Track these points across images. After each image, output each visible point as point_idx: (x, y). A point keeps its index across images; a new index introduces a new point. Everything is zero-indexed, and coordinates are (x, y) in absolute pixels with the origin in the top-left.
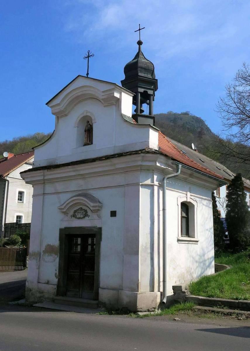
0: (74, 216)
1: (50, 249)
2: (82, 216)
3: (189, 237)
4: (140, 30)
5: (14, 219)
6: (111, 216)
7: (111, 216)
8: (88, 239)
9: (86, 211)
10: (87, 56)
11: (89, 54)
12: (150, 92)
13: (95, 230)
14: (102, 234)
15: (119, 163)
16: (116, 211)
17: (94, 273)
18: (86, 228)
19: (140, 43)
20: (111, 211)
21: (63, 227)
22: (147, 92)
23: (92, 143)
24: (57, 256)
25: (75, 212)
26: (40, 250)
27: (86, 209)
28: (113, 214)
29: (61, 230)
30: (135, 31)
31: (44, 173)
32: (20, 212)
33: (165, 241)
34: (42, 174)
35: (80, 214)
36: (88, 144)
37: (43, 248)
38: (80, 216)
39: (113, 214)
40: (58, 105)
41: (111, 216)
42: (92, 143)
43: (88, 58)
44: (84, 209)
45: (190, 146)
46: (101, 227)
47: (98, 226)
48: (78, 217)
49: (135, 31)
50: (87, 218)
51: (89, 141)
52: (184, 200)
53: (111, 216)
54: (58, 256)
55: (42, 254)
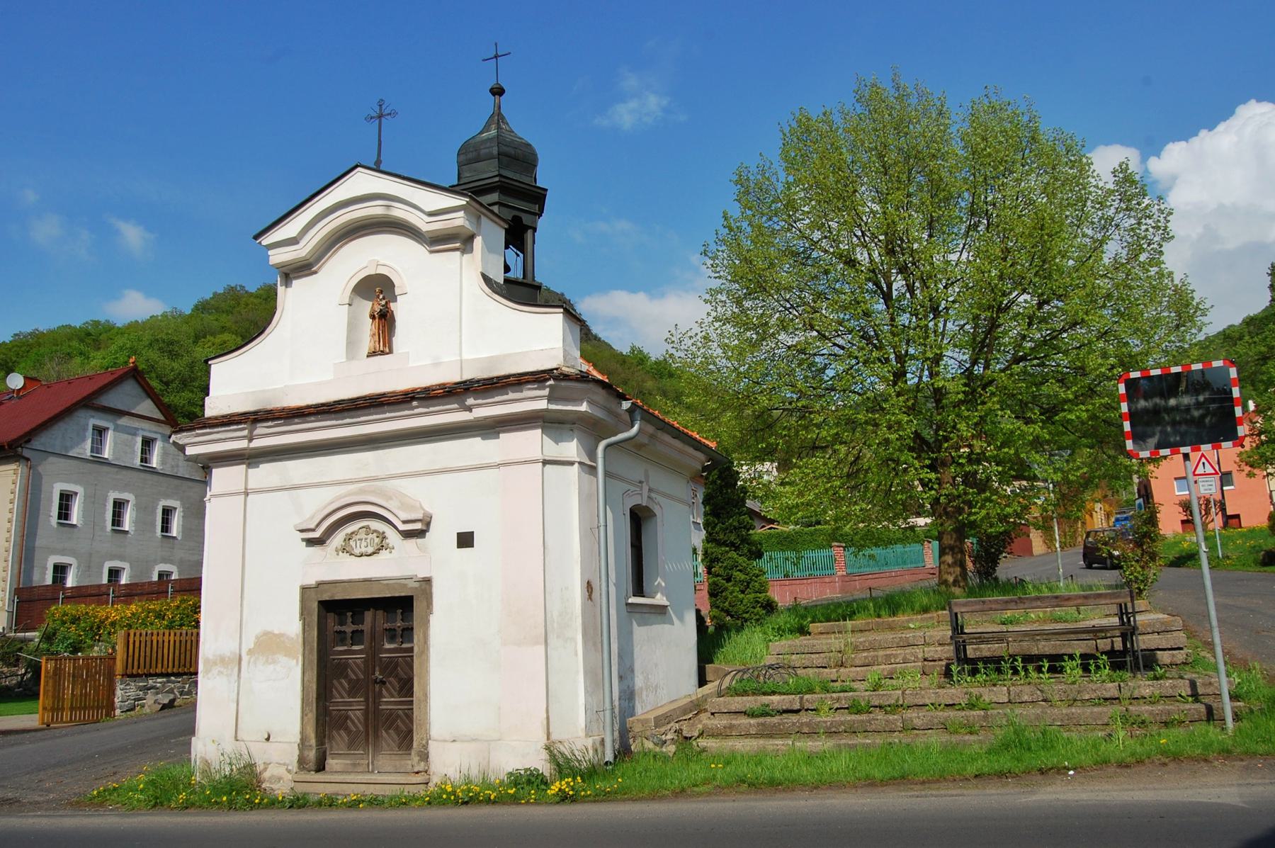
1: (268, 644)
2: (370, 550)
3: (643, 596)
4: (496, 57)
5: (45, 574)
6: (459, 535)
9: (383, 537)
10: (375, 115)
11: (381, 110)
12: (526, 219)
13: (412, 584)
14: (434, 596)
16: (473, 532)
17: (412, 701)
18: (456, 406)
19: (498, 91)
21: (311, 581)
22: (520, 219)
23: (391, 352)
24: (295, 661)
25: (349, 538)
26: (240, 649)
27: (381, 531)
28: (465, 540)
29: (304, 589)
30: (484, 60)
31: (251, 432)
32: (63, 552)
35: (364, 544)
36: (383, 353)
37: (249, 643)
38: (363, 550)
39: (465, 540)
40: (293, 241)
41: (458, 547)
42: (391, 352)
43: (377, 121)
44: (375, 531)
45: (201, 403)
46: (428, 576)
47: (422, 574)
48: (357, 551)
49: (484, 60)
50: (384, 554)
51: (384, 345)
52: (636, 500)
53: (459, 535)
55: (245, 658)
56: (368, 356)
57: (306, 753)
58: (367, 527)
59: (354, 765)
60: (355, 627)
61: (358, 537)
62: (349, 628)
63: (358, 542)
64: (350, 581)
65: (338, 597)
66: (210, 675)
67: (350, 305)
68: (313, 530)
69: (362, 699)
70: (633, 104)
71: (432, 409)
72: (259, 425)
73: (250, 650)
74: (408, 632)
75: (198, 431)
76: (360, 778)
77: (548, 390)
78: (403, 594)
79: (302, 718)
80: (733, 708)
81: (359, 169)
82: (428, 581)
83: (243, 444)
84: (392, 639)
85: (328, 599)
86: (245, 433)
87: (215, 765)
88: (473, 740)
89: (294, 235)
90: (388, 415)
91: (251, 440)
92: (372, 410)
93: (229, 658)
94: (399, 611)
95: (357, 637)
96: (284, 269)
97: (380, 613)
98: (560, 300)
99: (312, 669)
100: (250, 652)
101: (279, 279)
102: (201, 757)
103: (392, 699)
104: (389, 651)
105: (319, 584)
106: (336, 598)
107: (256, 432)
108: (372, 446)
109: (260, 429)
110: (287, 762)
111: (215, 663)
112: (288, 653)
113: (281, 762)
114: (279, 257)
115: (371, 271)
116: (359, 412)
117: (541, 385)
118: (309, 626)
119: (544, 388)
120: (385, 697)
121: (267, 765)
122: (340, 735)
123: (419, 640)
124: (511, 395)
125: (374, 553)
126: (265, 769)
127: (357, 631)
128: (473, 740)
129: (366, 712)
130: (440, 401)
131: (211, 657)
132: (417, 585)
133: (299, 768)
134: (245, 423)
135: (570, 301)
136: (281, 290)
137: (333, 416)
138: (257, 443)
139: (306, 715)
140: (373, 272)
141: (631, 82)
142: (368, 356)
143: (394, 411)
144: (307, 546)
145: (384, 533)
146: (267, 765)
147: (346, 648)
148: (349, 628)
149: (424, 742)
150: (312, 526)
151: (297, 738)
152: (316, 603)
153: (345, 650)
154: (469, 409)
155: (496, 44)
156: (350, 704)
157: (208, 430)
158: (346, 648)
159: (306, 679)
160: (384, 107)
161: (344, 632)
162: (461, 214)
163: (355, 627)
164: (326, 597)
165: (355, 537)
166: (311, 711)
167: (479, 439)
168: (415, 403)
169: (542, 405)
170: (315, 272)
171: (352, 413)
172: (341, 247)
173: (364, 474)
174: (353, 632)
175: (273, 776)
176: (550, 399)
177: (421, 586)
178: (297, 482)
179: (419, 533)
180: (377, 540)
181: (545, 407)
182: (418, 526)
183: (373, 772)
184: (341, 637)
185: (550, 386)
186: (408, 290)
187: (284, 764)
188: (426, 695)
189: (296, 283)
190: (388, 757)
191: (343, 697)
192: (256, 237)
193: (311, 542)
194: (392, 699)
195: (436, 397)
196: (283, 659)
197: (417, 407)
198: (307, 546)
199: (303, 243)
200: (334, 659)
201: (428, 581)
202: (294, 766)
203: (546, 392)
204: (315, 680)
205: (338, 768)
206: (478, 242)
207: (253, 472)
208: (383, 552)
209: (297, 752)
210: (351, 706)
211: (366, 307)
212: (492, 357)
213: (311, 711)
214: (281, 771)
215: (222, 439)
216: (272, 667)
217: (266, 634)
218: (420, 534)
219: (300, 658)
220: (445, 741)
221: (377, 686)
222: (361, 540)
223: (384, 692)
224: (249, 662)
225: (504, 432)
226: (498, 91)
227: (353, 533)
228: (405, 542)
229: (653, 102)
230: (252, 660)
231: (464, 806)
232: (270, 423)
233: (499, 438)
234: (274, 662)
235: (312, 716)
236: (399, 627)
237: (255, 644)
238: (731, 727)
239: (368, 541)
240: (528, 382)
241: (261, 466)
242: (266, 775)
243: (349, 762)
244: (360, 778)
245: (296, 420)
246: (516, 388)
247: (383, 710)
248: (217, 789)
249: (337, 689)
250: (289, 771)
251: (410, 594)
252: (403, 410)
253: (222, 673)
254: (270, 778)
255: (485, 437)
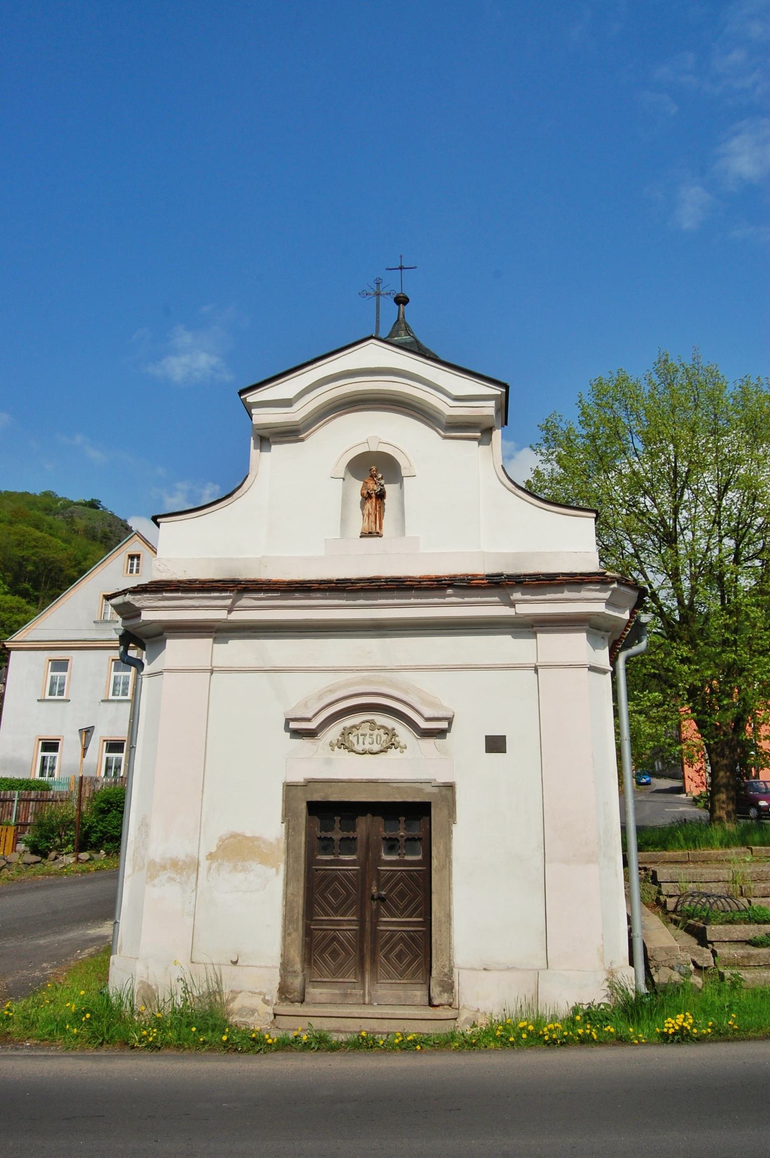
0: (343, 744)
2: (376, 748)
4: (401, 268)
6: (488, 738)
7: (486, 736)
8: (383, 859)
9: (391, 733)
11: (378, 288)
13: (428, 789)
15: (359, 669)
16: (486, 736)
18: (496, 599)
20: (486, 752)
24: (274, 870)
25: (347, 732)
27: (390, 728)
28: (496, 744)
29: (289, 787)
30: (388, 269)
33: (469, 589)
34: (228, 602)
35: (368, 740)
38: (367, 747)
40: (287, 403)
44: (383, 727)
47: (442, 779)
53: (488, 738)
54: (277, 870)
55: (204, 864)
56: (361, 537)
57: (289, 980)
58: (372, 722)
59: (346, 995)
60: (345, 834)
61: (360, 732)
62: (337, 835)
63: (361, 738)
64: (350, 781)
65: (334, 798)
66: (156, 881)
67: (344, 479)
68: (308, 720)
69: (355, 918)
70: (185, 359)
71: (467, 600)
72: (246, 595)
73: (211, 854)
74: (425, 843)
75: (165, 594)
76: (356, 1011)
77: (609, 593)
78: (418, 800)
79: (284, 939)
80: (735, 937)
81: (373, 341)
82: (450, 787)
83: (222, 615)
84: (391, 849)
85: (319, 799)
86: (228, 602)
87: (163, 994)
88: (509, 969)
89: (291, 397)
90: (413, 601)
91: (230, 612)
92: (396, 593)
93: (184, 862)
94: (402, 819)
95: (348, 845)
96: (262, 432)
97: (379, 820)
98: (122, 526)
99: (298, 881)
100: (211, 856)
101: (252, 441)
102: (142, 982)
103: (394, 919)
104: (390, 863)
105: (309, 782)
106: (331, 799)
107: (239, 603)
108: (379, 633)
109: (246, 601)
110: (265, 991)
111: (164, 868)
112: (265, 860)
113: (257, 991)
114: (262, 417)
115: (364, 449)
116: (379, 594)
117: (604, 587)
118: (294, 829)
119: (605, 591)
120: (384, 917)
121: (235, 993)
122: (324, 960)
123: (438, 853)
124: (567, 594)
125: (382, 751)
126: (233, 999)
127: (348, 838)
128: (509, 969)
129: (361, 932)
130: (480, 592)
131: (158, 860)
132: (435, 790)
133: (280, 998)
134: (232, 591)
135: (131, 527)
136: (254, 453)
137: (554, 589)
138: (236, 616)
139: (289, 934)
140: (373, 449)
141: (187, 339)
142: (361, 537)
143: (387, 598)
144: (291, 737)
145: (394, 729)
146: (235, 993)
147: (331, 857)
148: (337, 835)
149: (446, 970)
150: (309, 715)
151: (277, 961)
152: (304, 804)
153: (332, 861)
154: (512, 605)
155: (401, 257)
156: (339, 922)
157: (180, 595)
158: (331, 857)
159: (289, 892)
160: (381, 286)
161: (331, 839)
162: (492, 403)
163: (345, 834)
164: (317, 797)
165: (355, 732)
166: (296, 930)
167: (509, 637)
168: (449, 591)
169: (600, 608)
170: (302, 440)
171: (369, 594)
172: (334, 418)
173: (365, 663)
174: (342, 839)
175: (243, 1007)
176: (609, 603)
177: (440, 792)
178: (279, 664)
179: (439, 733)
180: (384, 737)
181: (226, 618)
182: (444, 725)
183: (370, 1004)
184: (326, 845)
185: (614, 590)
186: (416, 472)
187: (260, 993)
188: (449, 917)
189: (277, 450)
190: (388, 986)
191: (327, 915)
192: (241, 393)
193: (297, 734)
194: (394, 919)
195: (478, 587)
196: (257, 867)
197: (450, 596)
198: (291, 737)
199: (296, 406)
200: (317, 870)
201: (450, 787)
202: (273, 995)
203: (607, 595)
204: (301, 893)
205: (323, 999)
206: (497, 434)
207: (218, 647)
208: (392, 751)
209: (278, 979)
210: (340, 925)
211: (357, 486)
212: (519, 553)
213: (296, 930)
214: (257, 1002)
215: (193, 607)
216: (241, 876)
217: (234, 836)
218: (441, 733)
219: (282, 867)
220: (473, 969)
221: (374, 904)
222: (364, 735)
223: (383, 910)
224: (210, 869)
225: (542, 632)
226: (401, 301)
227: (354, 727)
228: (420, 741)
229: (204, 361)
230: (214, 866)
231: (562, 1048)
232: (262, 595)
233: (227, 643)
234: (245, 870)
235: (297, 936)
236: (402, 837)
237: (219, 847)
238: (749, 957)
239: (374, 737)
240: (591, 583)
241: (230, 642)
242: (235, 1005)
243: (337, 992)
244: (356, 1011)
245: (297, 595)
246: (575, 587)
247: (381, 931)
248: (489, 1032)
249: (320, 906)
250: (266, 1002)
251: (427, 800)
252: (433, 597)
253: (173, 879)
254: (240, 1010)
255: (516, 636)
